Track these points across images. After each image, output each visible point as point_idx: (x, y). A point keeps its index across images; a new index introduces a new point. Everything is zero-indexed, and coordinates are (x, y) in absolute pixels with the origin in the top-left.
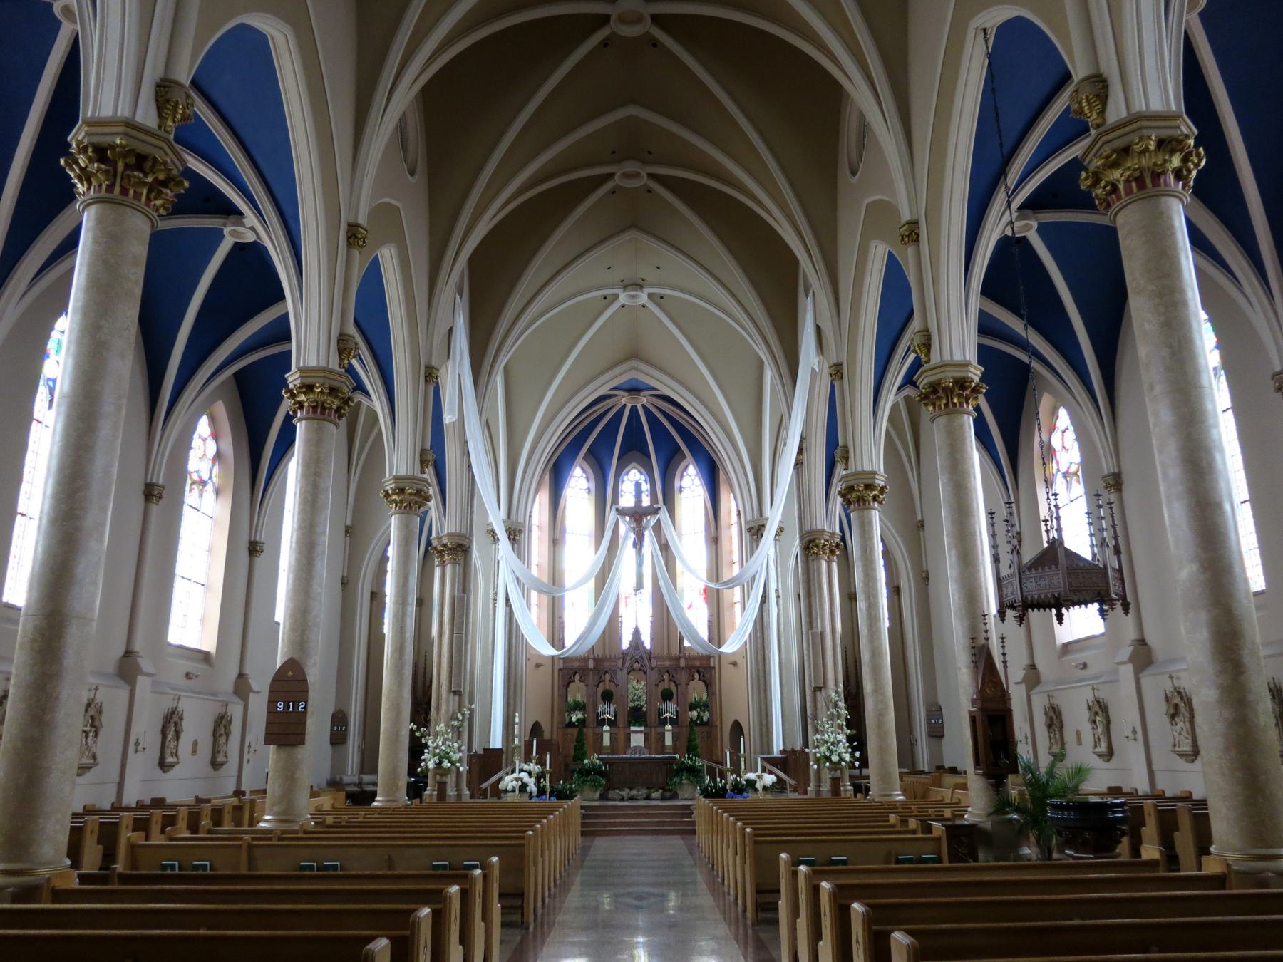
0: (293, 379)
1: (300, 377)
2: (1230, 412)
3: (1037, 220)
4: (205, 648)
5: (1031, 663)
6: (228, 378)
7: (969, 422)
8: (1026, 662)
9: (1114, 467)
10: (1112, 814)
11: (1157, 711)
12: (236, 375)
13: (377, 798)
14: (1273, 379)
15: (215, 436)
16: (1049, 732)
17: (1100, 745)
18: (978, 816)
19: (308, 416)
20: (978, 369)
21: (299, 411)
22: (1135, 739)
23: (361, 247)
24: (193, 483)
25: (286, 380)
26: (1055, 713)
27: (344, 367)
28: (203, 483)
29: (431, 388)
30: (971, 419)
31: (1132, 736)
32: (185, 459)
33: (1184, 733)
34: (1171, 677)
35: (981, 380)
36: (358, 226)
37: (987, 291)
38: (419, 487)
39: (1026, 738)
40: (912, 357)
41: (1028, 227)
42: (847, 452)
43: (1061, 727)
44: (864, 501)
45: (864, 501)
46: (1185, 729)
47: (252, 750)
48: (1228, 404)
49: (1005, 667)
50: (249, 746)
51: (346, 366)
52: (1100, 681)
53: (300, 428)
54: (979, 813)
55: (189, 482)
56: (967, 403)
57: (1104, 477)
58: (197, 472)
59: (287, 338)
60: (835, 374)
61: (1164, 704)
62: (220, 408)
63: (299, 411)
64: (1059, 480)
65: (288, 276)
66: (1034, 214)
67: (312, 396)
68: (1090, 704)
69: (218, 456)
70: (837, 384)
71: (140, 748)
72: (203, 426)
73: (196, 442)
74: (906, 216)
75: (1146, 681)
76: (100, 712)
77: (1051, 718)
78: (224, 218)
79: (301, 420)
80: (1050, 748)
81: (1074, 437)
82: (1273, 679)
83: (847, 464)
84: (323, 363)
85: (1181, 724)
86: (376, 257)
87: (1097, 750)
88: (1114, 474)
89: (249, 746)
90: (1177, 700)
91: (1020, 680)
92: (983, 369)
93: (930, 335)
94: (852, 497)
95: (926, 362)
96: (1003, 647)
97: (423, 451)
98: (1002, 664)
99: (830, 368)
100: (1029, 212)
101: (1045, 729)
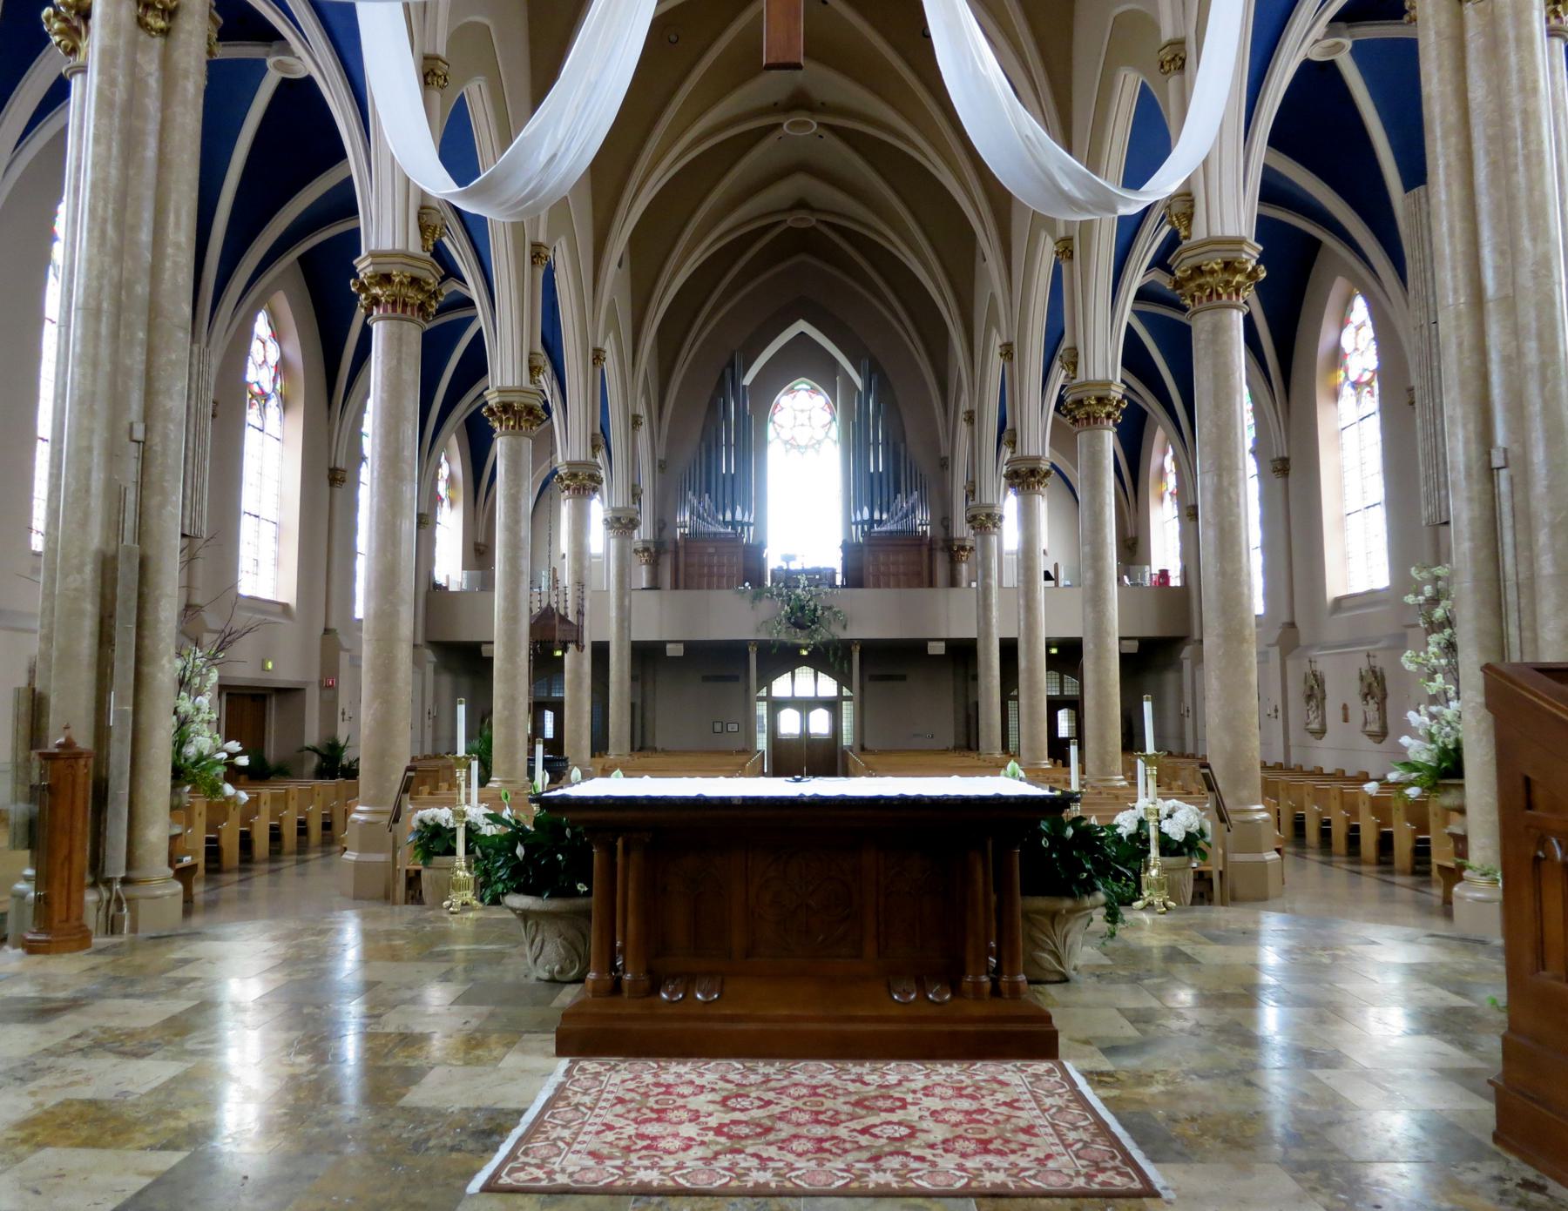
0: (364, 266)
1: (372, 264)
2: (1256, 478)
3: (1352, 37)
6: (292, 264)
7: (1238, 318)
11: (1296, 691)
12: (301, 259)
13: (492, 779)
15: (277, 336)
19: (385, 315)
20: (1254, 248)
21: (374, 308)
23: (442, 87)
25: (355, 268)
26: (1316, 681)
27: (428, 250)
28: (265, 397)
29: (540, 272)
30: (1241, 315)
31: (1273, 714)
32: (243, 370)
34: (1310, 661)
35: (1259, 262)
36: (437, 58)
37: (1277, 140)
38: (592, 472)
39: (1276, 711)
40: (1167, 229)
41: (1338, 47)
42: (1015, 435)
44: (1096, 419)
45: (1096, 419)
47: (346, 717)
50: (343, 713)
51: (431, 248)
52: (1377, 646)
53: (379, 331)
56: (1238, 294)
57: (1274, 461)
58: (258, 383)
59: (354, 211)
60: (1063, 252)
62: (281, 302)
63: (374, 308)
64: (1347, 391)
65: (474, 279)
66: (1349, 27)
67: (389, 288)
68: (1364, 673)
70: (1065, 267)
72: (262, 326)
73: (256, 346)
74: (1167, 34)
75: (1290, 663)
77: (1370, 685)
78: (267, 45)
79: (377, 320)
81: (1372, 335)
83: (1014, 447)
84: (399, 246)
85: (1372, 705)
86: (462, 100)
89: (343, 713)
92: (1261, 248)
93: (1193, 200)
95: (1186, 238)
97: (594, 435)
99: (1056, 244)
100: (1342, 25)
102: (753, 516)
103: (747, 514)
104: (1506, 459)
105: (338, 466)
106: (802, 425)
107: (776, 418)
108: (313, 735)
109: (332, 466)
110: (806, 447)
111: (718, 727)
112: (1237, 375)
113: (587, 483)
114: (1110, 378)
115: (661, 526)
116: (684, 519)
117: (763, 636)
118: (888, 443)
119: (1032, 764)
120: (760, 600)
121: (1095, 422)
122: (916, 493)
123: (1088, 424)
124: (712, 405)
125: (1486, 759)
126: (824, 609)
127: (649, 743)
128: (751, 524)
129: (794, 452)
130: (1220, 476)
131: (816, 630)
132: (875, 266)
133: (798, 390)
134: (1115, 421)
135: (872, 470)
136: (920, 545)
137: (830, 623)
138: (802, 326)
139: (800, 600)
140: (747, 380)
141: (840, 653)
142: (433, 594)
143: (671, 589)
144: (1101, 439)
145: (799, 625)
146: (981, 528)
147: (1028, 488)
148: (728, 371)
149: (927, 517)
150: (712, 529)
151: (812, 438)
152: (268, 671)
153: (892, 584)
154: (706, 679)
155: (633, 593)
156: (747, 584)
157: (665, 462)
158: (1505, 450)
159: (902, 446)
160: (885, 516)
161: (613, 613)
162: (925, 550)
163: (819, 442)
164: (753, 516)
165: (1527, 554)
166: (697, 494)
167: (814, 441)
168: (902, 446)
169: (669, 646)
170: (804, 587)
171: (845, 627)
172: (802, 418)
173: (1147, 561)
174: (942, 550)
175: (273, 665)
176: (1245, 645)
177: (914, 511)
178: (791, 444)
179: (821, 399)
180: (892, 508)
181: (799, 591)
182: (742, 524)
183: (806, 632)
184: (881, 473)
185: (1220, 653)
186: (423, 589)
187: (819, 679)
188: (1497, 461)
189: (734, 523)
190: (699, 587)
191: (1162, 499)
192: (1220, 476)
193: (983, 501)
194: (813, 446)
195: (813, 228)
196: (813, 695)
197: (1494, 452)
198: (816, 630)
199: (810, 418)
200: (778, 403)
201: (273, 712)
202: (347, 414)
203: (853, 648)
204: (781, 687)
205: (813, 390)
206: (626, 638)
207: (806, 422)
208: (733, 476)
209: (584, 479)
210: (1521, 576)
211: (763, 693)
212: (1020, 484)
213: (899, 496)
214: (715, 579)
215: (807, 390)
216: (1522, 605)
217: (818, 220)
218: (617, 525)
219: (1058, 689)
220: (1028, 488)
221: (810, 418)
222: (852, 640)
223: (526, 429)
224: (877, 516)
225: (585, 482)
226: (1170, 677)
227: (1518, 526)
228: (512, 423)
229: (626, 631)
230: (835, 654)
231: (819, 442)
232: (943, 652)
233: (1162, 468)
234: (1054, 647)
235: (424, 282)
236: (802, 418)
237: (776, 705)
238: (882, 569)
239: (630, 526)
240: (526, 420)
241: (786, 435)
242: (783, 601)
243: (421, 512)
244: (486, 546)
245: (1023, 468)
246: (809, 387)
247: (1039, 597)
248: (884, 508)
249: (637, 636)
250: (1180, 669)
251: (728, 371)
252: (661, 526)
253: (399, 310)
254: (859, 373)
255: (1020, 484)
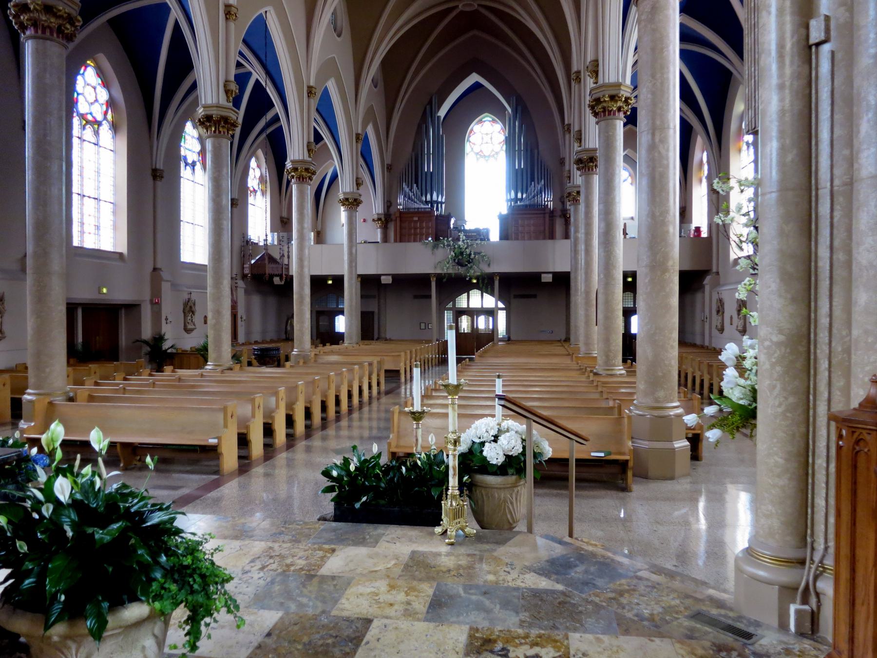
4: (119, 250)
13: (209, 363)
24: (251, 192)
28: (255, 191)
38: (307, 166)
43: (724, 313)
44: (610, 112)
50: (241, 318)
55: (249, 192)
60: (576, 79)
62: (260, 153)
69: (111, 103)
71: (168, 321)
72: (253, 163)
76: (194, 304)
77: (719, 307)
89: (241, 318)
94: (598, 109)
102: (444, 197)
103: (440, 196)
104: (827, 30)
105: (158, 167)
106: (487, 143)
107: (471, 139)
108: (147, 333)
109: (154, 167)
110: (489, 156)
111: (423, 326)
112: (671, 47)
113: (304, 174)
114: (621, 81)
115: (389, 204)
116: (400, 201)
117: (439, 271)
118: (527, 150)
119: (586, 353)
120: (437, 248)
121: (609, 114)
122: (543, 181)
123: (605, 115)
124: (419, 127)
125: (791, 400)
126: (475, 254)
127: (383, 335)
128: (443, 203)
129: (482, 160)
130: (653, 135)
131: (471, 267)
132: (512, 29)
133: (485, 121)
134: (625, 113)
135: (517, 167)
136: (544, 214)
137: (479, 262)
138: (474, 78)
139: (461, 249)
140: (442, 113)
141: (486, 281)
142: (246, 246)
143: (395, 241)
144: (614, 128)
145: (460, 264)
146: (573, 201)
147: (589, 170)
148: (428, 107)
149: (550, 198)
150: (416, 206)
151: (493, 150)
152: (104, 294)
153: (526, 238)
154: (416, 297)
155: (358, 245)
156: (430, 239)
157: (390, 165)
158: (827, 18)
159: (536, 151)
160: (524, 196)
161: (346, 257)
162: (547, 216)
163: (497, 153)
164: (444, 197)
165: (846, 152)
166: (410, 187)
167: (493, 153)
168: (536, 151)
169: (382, 278)
170: (463, 241)
171: (489, 265)
172: (487, 139)
173: (690, 222)
174: (560, 216)
175: (108, 290)
176: (667, 275)
177: (541, 193)
178: (480, 154)
179: (498, 126)
180: (529, 191)
181: (460, 243)
182: (437, 202)
183: (466, 268)
184: (522, 169)
185: (647, 281)
186: (237, 244)
187: (484, 297)
188: (816, 35)
189: (432, 202)
190: (409, 241)
191: (701, 181)
192: (653, 135)
193: (575, 184)
194: (493, 156)
195: (476, 11)
196: (480, 307)
197: (813, 23)
198: (471, 267)
199: (491, 138)
200: (472, 130)
201: (123, 315)
202: (161, 138)
203: (495, 278)
204: (462, 302)
205: (494, 121)
206: (354, 273)
207: (489, 141)
208: (431, 173)
209: (301, 171)
210: (837, 182)
211: (450, 305)
212: (583, 167)
213: (533, 183)
214: (412, 236)
215: (490, 121)
216: (836, 220)
217: (479, 5)
218: (347, 203)
219: (632, 303)
220: (589, 170)
221: (491, 138)
222: (494, 273)
223: (224, 133)
224: (519, 195)
225: (303, 173)
226: (699, 296)
227: (836, 117)
228: (213, 129)
229: (354, 269)
230: (483, 282)
231: (497, 153)
232: (551, 281)
233: (701, 161)
234: (630, 277)
235: (56, 9)
236: (487, 139)
237: (460, 313)
238: (520, 229)
239: (355, 203)
240: (223, 127)
241: (477, 149)
242: (451, 249)
243: (233, 197)
244: (288, 219)
245: (585, 157)
246: (491, 119)
247: (594, 244)
248: (524, 190)
249: (362, 271)
250: (704, 292)
251: (428, 107)
252: (389, 204)
253: (40, 32)
254: (510, 106)
255: (583, 167)
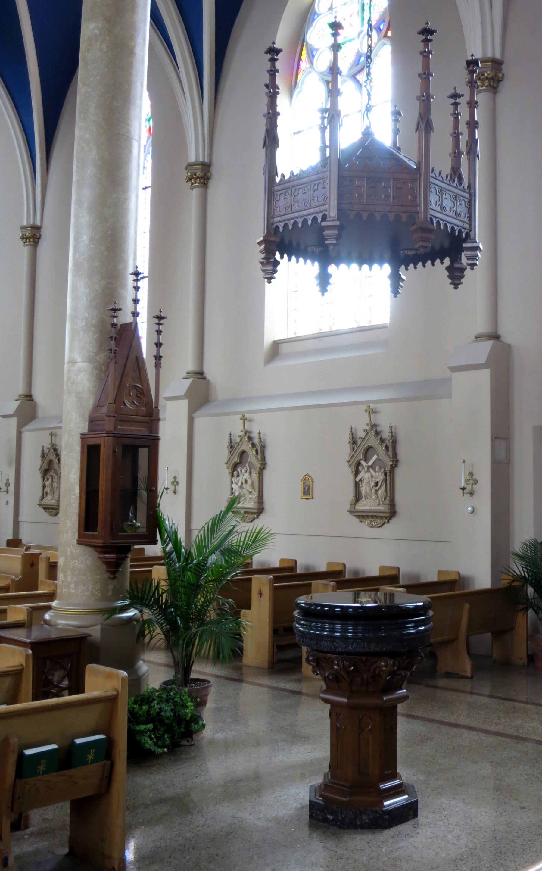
2: (149, 190)
5: (26, 393)
8: (21, 390)
9: (204, 157)
10: (414, 627)
14: (186, 169)
16: (44, 479)
17: (371, 496)
18: (74, 617)
22: (175, 492)
31: (171, 488)
33: (248, 487)
43: (263, 466)
46: (249, 482)
48: (149, 183)
49: (158, 366)
54: (72, 610)
57: (22, 228)
61: (225, 451)
75: (200, 422)
80: (43, 498)
82: (259, 433)
87: (359, 507)
88: (203, 164)
90: (246, 446)
91: (11, 412)
96: (159, 332)
98: (154, 361)
101: (39, 476)
